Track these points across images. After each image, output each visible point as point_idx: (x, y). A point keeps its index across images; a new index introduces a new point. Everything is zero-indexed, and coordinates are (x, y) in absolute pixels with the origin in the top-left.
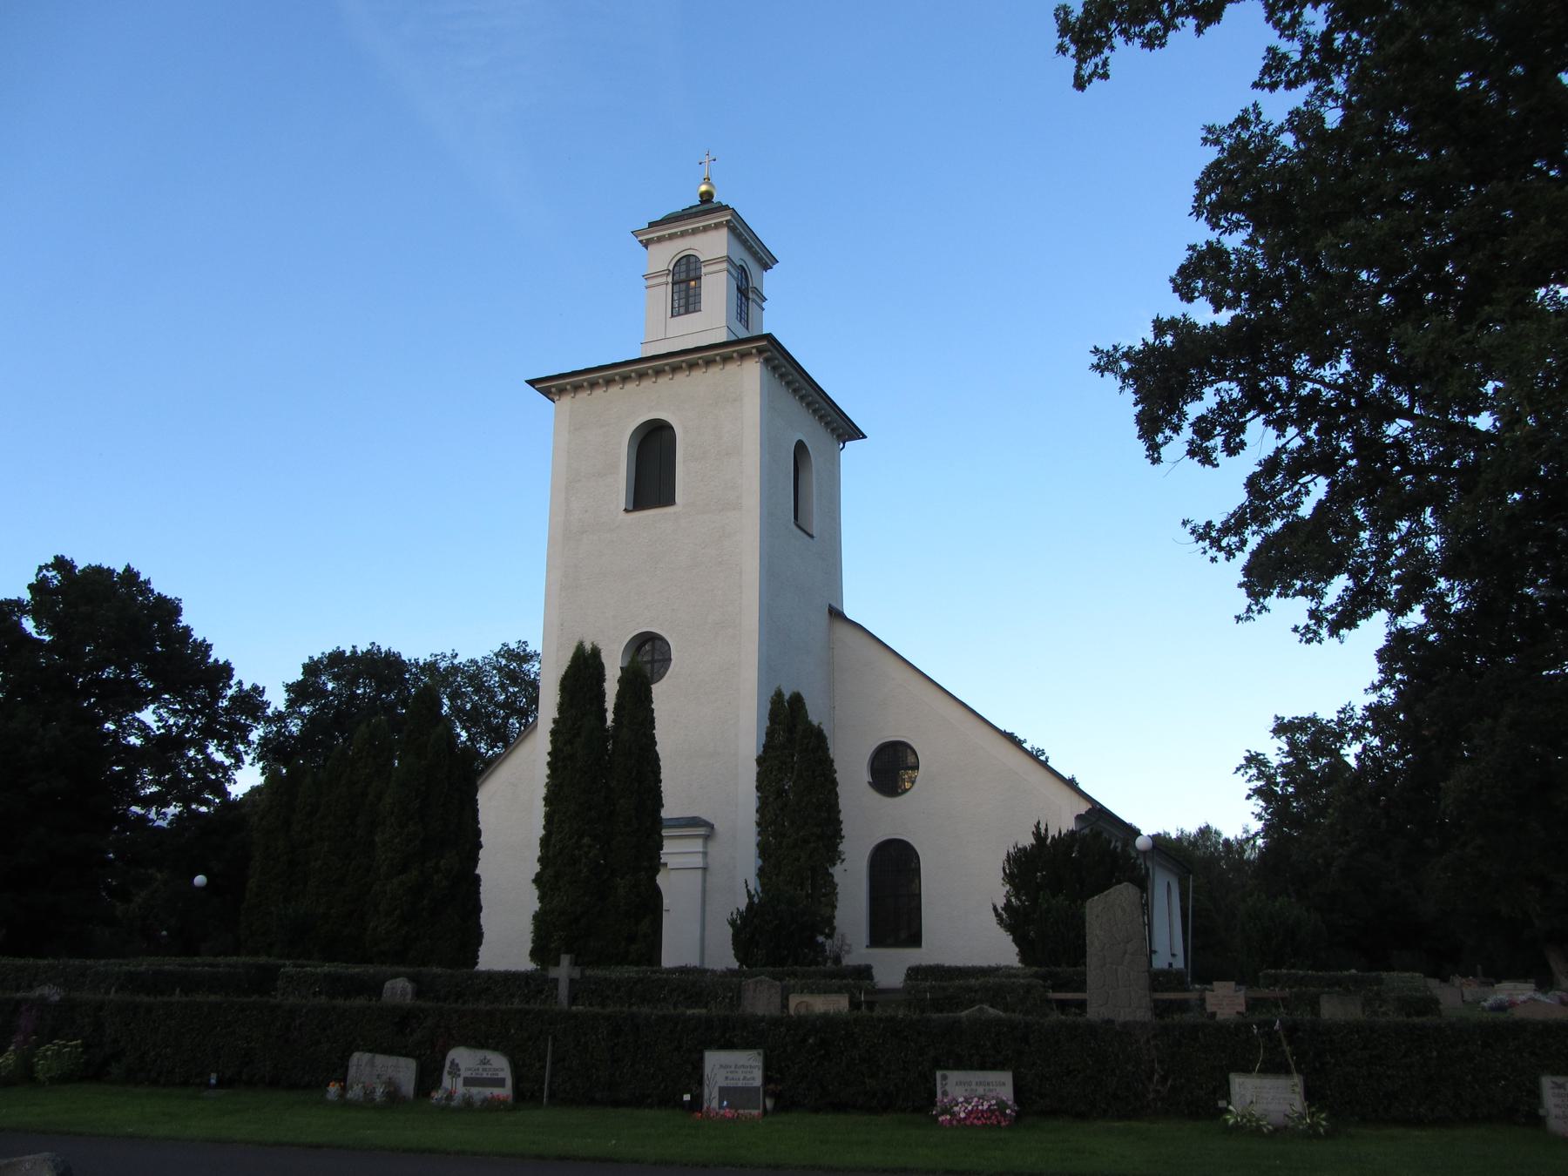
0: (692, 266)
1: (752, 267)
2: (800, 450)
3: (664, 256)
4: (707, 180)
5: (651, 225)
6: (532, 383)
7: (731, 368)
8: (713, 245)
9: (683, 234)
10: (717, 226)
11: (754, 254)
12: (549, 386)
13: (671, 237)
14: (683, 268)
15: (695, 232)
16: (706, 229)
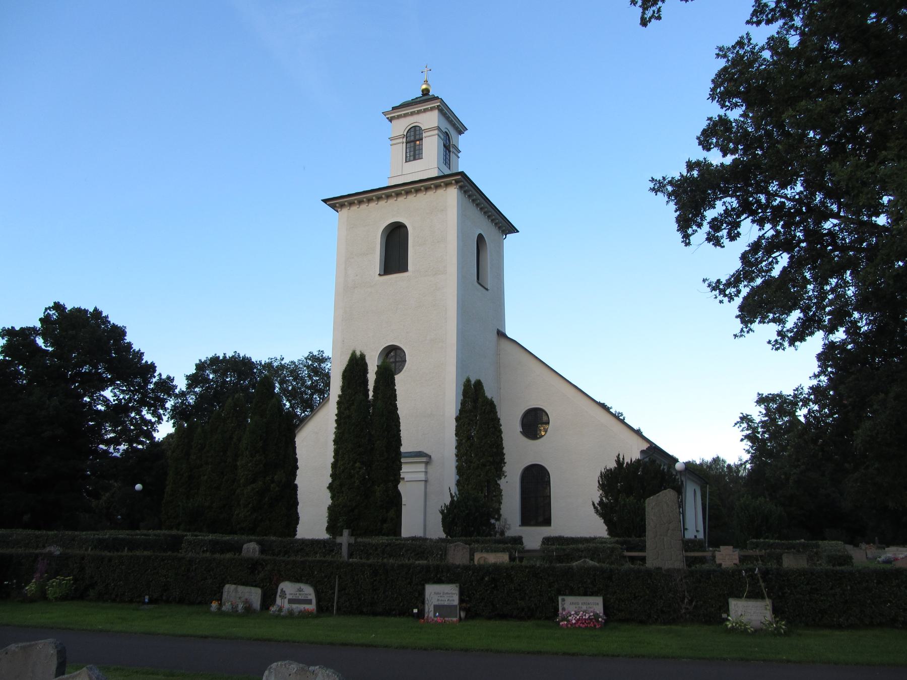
0: (418, 133)
1: (453, 133)
3: (401, 126)
4: (426, 82)
5: (394, 108)
8: (430, 120)
9: (412, 114)
10: (432, 109)
11: (454, 125)
12: (335, 203)
13: (405, 115)
14: (412, 133)
15: (419, 112)
16: (425, 111)
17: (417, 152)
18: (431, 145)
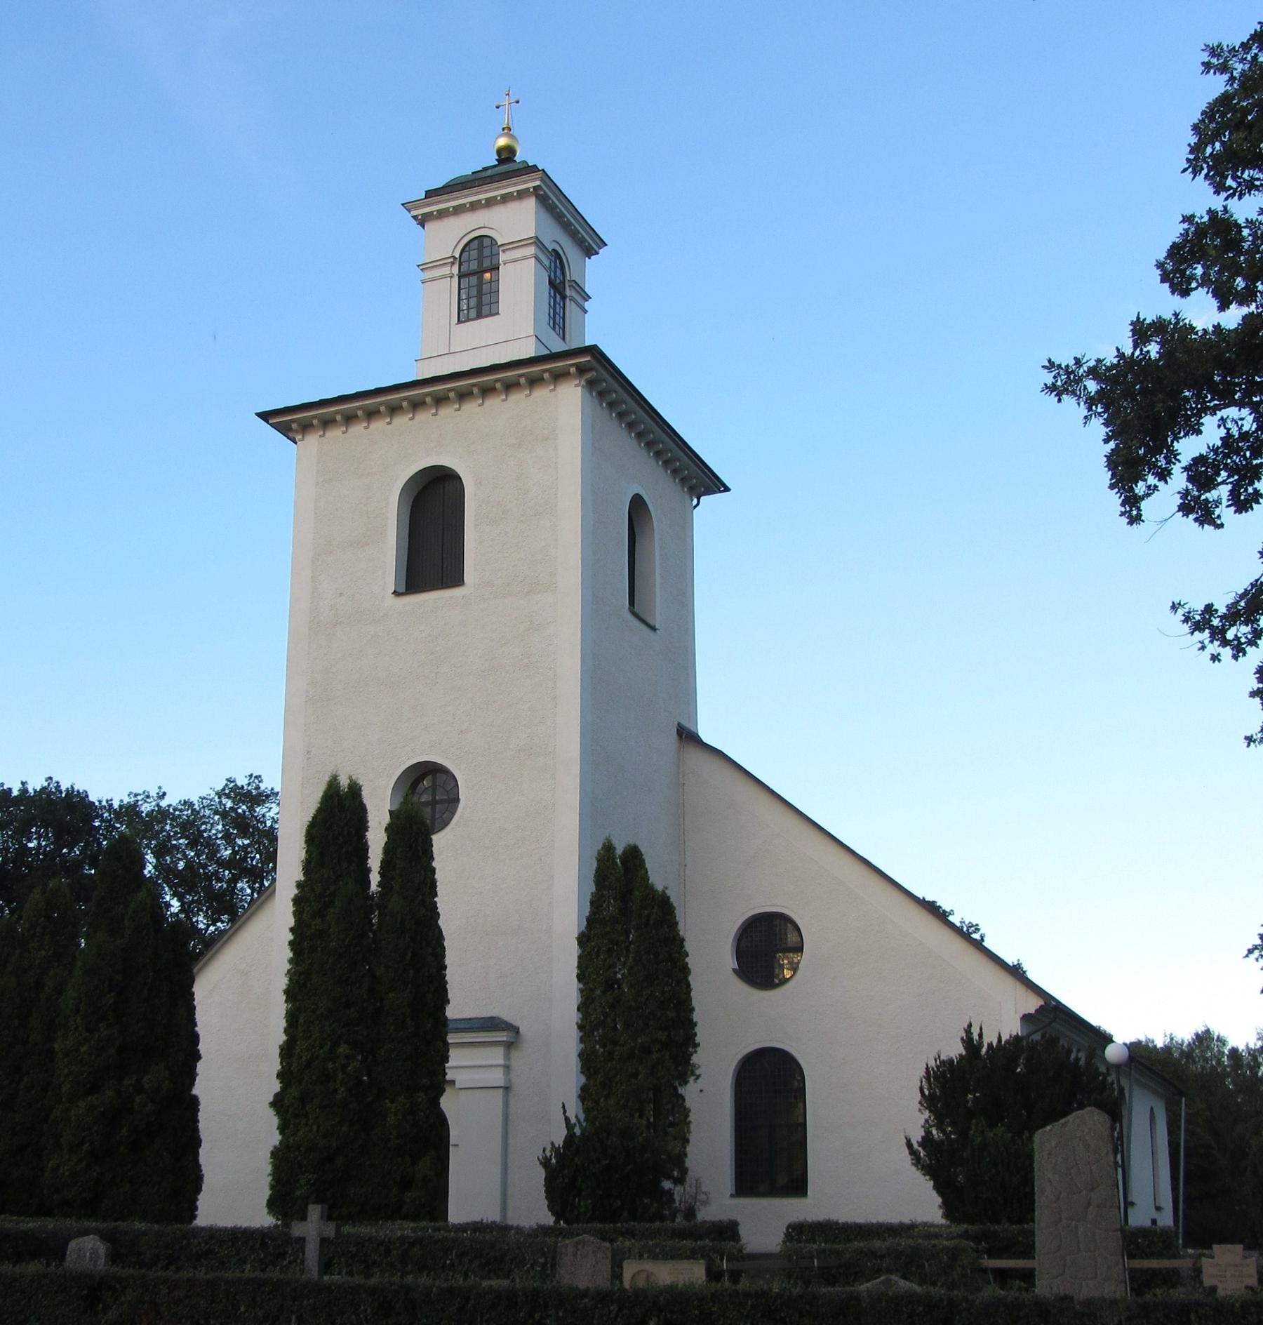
0: (487, 252)
1: (571, 252)
2: (638, 507)
3: (448, 237)
4: (507, 130)
5: (430, 194)
6: (727, 489)
7: (541, 393)
9: (474, 207)
10: (521, 195)
11: (573, 234)
12: (290, 421)
13: (457, 211)
14: (474, 254)
15: (490, 203)
16: (506, 199)
17: (486, 299)
18: (520, 283)
